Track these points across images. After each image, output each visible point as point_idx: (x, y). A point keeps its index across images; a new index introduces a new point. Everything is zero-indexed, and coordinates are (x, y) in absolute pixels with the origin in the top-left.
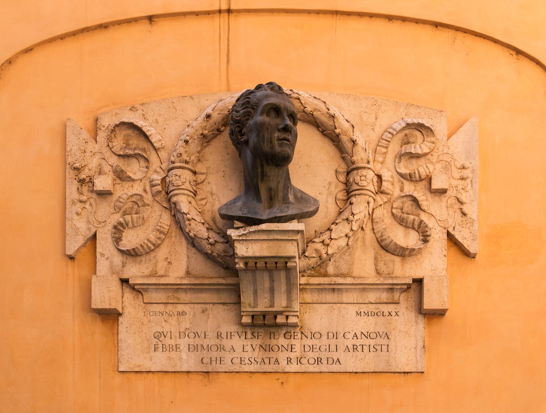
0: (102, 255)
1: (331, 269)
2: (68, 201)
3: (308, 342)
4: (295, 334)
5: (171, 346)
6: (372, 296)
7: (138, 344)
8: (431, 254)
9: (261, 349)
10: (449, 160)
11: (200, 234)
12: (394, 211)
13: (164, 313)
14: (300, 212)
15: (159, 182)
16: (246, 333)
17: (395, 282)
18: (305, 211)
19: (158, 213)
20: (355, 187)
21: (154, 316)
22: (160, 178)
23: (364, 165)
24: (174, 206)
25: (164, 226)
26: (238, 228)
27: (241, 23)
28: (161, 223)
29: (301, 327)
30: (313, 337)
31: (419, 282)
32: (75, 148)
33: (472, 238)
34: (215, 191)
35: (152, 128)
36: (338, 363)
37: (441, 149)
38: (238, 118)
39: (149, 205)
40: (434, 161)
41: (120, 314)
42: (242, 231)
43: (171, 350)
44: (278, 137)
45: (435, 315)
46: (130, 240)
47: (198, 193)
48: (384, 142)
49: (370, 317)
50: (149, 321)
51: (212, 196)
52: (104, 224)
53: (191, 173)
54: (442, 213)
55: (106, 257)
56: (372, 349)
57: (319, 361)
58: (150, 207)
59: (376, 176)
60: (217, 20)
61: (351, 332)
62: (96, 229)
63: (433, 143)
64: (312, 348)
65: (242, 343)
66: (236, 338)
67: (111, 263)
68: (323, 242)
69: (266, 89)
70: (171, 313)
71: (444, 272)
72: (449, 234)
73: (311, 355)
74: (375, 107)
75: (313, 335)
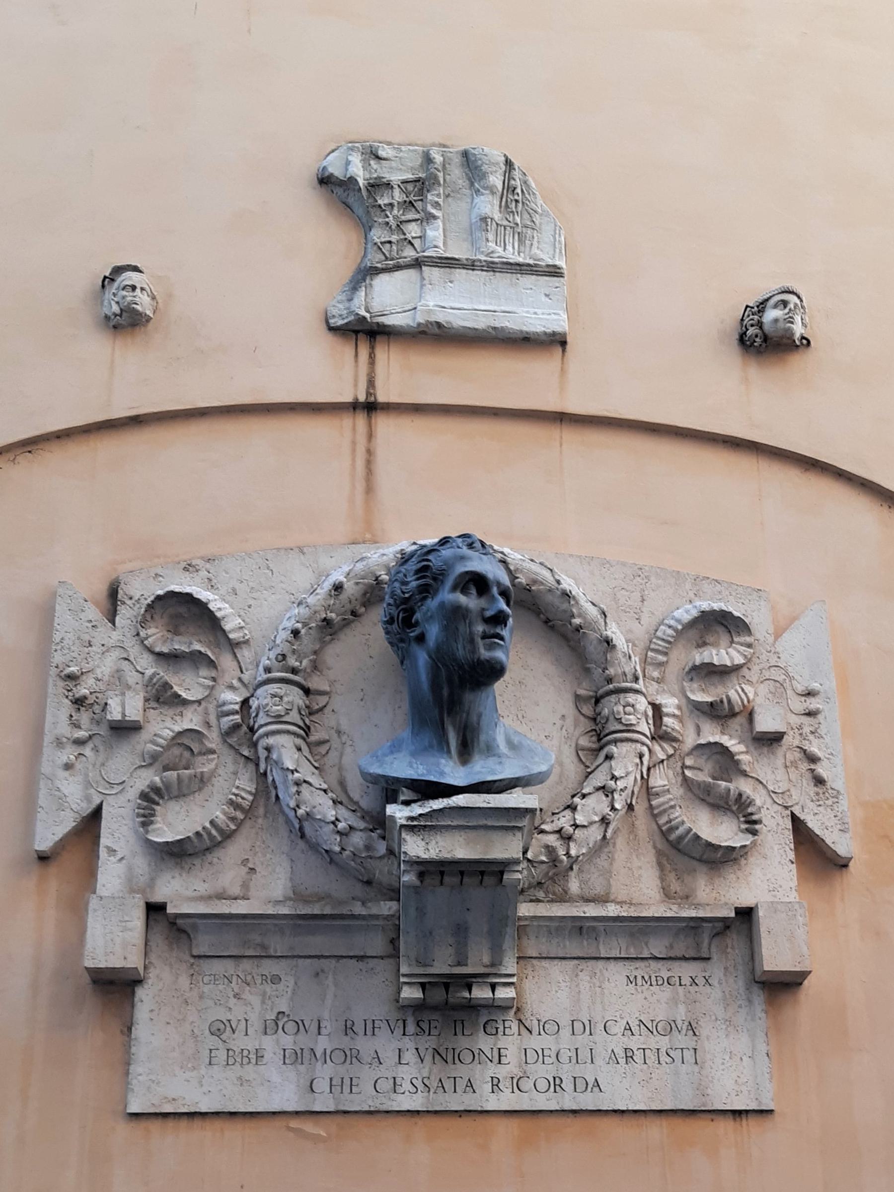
0: (111, 851)
1: (574, 886)
2: (48, 739)
3: (535, 1042)
4: (507, 1024)
5: (245, 1053)
6: (657, 947)
7: (174, 1049)
8: (765, 857)
9: (437, 1057)
10: (781, 678)
11: (319, 813)
12: (688, 773)
13: (235, 978)
14: (527, 774)
15: (237, 707)
16: (404, 1021)
17: (701, 914)
18: (535, 772)
19: (231, 767)
20: (613, 726)
21: (211, 986)
22: (239, 699)
23: (628, 685)
24: (265, 753)
25: (243, 794)
26: (407, 803)
27: (384, 424)
28: (238, 787)
29: (518, 1009)
30: (542, 1032)
31: (746, 914)
32: (69, 639)
33: (839, 826)
34: (345, 725)
35: (227, 605)
36: (596, 1089)
37: (764, 657)
38: (407, 595)
39: (213, 752)
40: (754, 679)
41: (139, 982)
42: (417, 810)
43: (245, 1060)
44: (484, 632)
45: (781, 987)
46: (175, 823)
47: (312, 728)
48: (660, 642)
49: (655, 988)
50: (201, 997)
51: (339, 736)
52: (120, 787)
53: (301, 692)
54: (778, 779)
55: (119, 856)
56: (664, 1058)
57: (556, 1084)
58: (215, 756)
59: (650, 707)
60: (347, 421)
61: (619, 1020)
62: (101, 797)
63: (749, 646)
64: (541, 1055)
65: (396, 1044)
66: (383, 1032)
67: (130, 868)
68: (559, 831)
69: (460, 545)
70: (249, 978)
71: (793, 897)
72: (794, 818)
73: (543, 1072)
74: (638, 579)
75: (543, 1026)
